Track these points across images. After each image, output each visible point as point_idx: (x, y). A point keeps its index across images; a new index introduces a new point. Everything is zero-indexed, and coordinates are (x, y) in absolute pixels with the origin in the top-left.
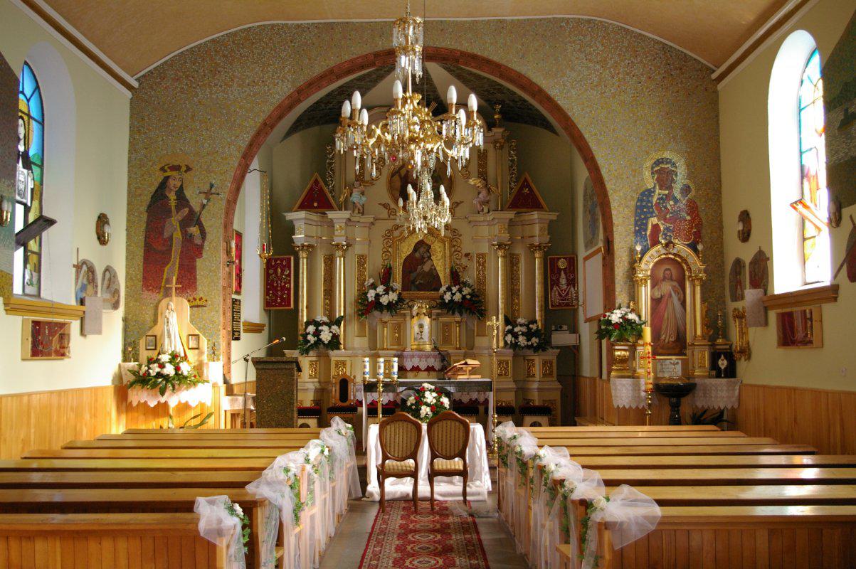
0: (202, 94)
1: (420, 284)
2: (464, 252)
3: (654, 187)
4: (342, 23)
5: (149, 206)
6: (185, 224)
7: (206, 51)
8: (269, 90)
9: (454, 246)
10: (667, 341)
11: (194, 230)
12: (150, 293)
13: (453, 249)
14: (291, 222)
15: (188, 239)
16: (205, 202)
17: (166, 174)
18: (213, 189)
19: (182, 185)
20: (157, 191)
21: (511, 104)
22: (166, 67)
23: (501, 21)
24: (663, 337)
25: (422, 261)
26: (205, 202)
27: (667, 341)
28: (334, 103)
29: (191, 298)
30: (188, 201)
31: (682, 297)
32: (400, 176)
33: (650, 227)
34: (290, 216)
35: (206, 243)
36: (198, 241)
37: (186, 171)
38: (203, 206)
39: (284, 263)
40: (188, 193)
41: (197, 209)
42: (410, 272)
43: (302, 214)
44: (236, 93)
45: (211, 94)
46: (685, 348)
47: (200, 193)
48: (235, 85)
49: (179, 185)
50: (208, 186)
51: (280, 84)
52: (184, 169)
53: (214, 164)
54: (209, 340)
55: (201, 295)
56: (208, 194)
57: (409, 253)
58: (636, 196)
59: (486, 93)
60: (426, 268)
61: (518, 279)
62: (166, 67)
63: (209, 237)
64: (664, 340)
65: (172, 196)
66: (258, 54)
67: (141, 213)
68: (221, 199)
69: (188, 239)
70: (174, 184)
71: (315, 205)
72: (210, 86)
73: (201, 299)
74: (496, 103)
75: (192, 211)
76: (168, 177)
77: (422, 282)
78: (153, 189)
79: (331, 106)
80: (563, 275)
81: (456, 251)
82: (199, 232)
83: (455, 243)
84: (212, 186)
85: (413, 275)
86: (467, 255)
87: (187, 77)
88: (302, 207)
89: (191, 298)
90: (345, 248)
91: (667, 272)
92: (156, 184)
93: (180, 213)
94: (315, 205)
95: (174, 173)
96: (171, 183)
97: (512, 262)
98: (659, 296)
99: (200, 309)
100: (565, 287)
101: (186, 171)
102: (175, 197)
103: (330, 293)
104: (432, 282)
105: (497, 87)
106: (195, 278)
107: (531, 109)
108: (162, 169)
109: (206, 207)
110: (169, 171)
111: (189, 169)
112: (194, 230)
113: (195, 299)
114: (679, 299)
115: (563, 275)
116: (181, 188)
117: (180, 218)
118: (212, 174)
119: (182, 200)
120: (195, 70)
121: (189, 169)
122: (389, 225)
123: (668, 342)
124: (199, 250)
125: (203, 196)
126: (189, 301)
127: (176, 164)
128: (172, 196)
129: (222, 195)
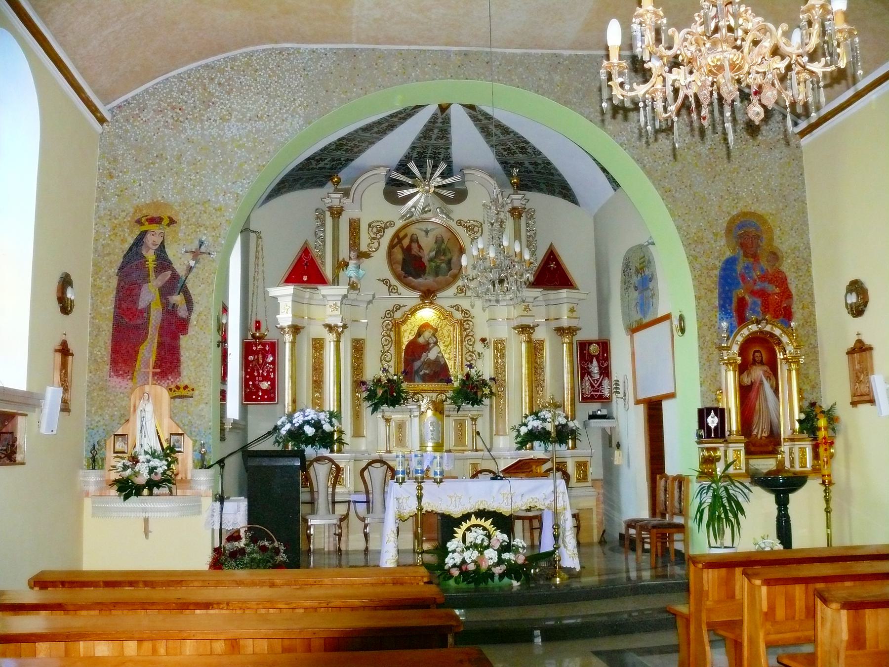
0: (191, 129)
1: (425, 374)
2: (478, 337)
4: (368, 49)
5: (121, 269)
6: (166, 291)
7: (198, 79)
8: (276, 125)
9: (466, 330)
10: (759, 436)
11: (177, 299)
12: (120, 379)
13: (465, 334)
14: (275, 298)
15: (170, 311)
16: (192, 263)
17: (143, 228)
18: (203, 247)
19: (162, 243)
20: (131, 249)
21: (531, 167)
22: (147, 96)
23: (556, 55)
24: (755, 433)
25: (426, 347)
26: (192, 263)
27: (759, 436)
28: (326, 162)
29: (173, 386)
30: (170, 263)
32: (402, 247)
33: (735, 300)
34: (274, 292)
35: (194, 317)
36: (182, 312)
37: (168, 225)
38: (190, 269)
39: (267, 348)
40: (170, 252)
41: (181, 271)
42: (414, 360)
43: (290, 289)
44: (234, 130)
45: (202, 128)
46: (779, 444)
47: (186, 252)
48: (233, 120)
50: (197, 243)
51: (290, 120)
53: (205, 216)
54: (195, 442)
55: (186, 382)
56: (196, 254)
57: (411, 338)
59: (505, 153)
60: (432, 355)
61: (542, 368)
62: (147, 96)
63: (196, 308)
65: (150, 256)
66: (263, 83)
67: (110, 277)
68: (213, 261)
69: (170, 311)
70: (152, 240)
71: (305, 278)
72: (202, 121)
73: (186, 387)
74: (512, 167)
75: (175, 277)
77: (427, 372)
78: (127, 246)
79: (322, 164)
80: (595, 362)
81: (467, 335)
82: (184, 302)
83: (466, 327)
84: (201, 243)
85: (417, 364)
86: (483, 340)
87: (173, 108)
88: (289, 280)
89: (173, 386)
90: (340, 330)
91: (757, 354)
92: (131, 241)
93: (159, 277)
94: (305, 278)
95: (153, 227)
96: (150, 239)
97: (535, 349)
98: (749, 383)
99: (185, 400)
100: (597, 376)
101: (168, 225)
102: (154, 257)
103: (318, 384)
104: (439, 372)
105: (522, 145)
106: (178, 361)
107: (552, 174)
108: (139, 222)
109: (194, 270)
110: (147, 223)
111: (172, 222)
112: (177, 299)
113: (178, 388)
114: (772, 387)
115: (595, 362)
116: (162, 245)
117: (160, 284)
118: (202, 229)
119: (163, 263)
120: (183, 100)
121: (172, 222)
122: (389, 305)
124: (182, 326)
125: (189, 256)
126: (170, 390)
127: (155, 215)
128: (150, 256)
129: (214, 255)
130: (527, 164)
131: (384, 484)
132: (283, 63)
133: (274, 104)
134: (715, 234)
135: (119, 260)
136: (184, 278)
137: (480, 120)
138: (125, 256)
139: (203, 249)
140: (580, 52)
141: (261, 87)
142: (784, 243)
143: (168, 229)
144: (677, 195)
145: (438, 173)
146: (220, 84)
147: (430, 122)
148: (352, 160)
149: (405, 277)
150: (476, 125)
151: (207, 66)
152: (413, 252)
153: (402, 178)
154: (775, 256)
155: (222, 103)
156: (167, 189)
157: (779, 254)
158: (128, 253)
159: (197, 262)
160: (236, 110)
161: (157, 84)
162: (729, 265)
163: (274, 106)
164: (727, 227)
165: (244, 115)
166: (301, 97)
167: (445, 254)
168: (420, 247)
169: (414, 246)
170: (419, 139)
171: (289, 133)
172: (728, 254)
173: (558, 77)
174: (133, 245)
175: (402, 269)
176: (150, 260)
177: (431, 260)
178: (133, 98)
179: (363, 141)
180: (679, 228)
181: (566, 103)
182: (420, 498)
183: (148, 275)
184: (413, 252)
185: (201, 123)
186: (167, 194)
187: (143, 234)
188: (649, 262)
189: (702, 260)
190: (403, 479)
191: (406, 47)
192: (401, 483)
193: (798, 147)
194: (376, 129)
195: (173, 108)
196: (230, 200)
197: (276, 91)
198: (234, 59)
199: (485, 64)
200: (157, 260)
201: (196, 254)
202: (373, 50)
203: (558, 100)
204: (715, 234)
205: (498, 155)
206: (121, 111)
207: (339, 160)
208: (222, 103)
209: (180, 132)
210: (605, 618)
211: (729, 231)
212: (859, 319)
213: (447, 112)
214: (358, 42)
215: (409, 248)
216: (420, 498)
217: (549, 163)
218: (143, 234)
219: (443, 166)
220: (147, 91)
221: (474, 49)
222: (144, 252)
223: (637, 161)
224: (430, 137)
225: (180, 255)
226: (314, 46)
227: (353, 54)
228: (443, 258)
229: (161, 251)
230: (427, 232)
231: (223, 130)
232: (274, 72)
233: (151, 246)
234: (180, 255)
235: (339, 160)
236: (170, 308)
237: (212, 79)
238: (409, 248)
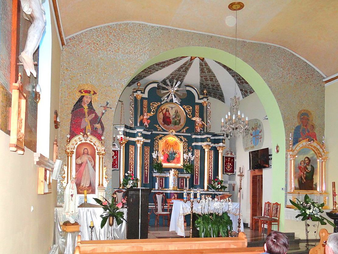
3: (301, 125)
5: (73, 111)
6: (93, 122)
17: (82, 95)
18: (108, 105)
20: (77, 103)
26: (104, 111)
30: (94, 110)
31: (93, 164)
32: (163, 113)
37: (93, 94)
40: (94, 106)
41: (99, 115)
48: (120, 52)
49: (90, 101)
51: (143, 55)
52: (92, 93)
56: (105, 108)
58: (294, 128)
64: (83, 186)
65: (86, 107)
68: (113, 111)
70: (86, 100)
72: (107, 51)
75: (96, 116)
76: (84, 96)
78: (75, 102)
87: (94, 43)
93: (90, 116)
95: (87, 94)
96: (85, 99)
101: (93, 94)
102: (87, 108)
108: (80, 91)
110: (84, 92)
111: (95, 93)
112: (98, 126)
114: (92, 165)
117: (90, 119)
119: (91, 109)
121: (95, 93)
123: (85, 187)
125: (103, 108)
128: (86, 107)
130: (210, 85)
131: (69, 202)
132: (140, 30)
133: (137, 48)
134: (294, 117)
135: (71, 107)
136: (100, 117)
137: (202, 66)
138: (74, 106)
139: (108, 106)
140: (253, 42)
141: (132, 40)
142: (316, 122)
143: (93, 96)
144: (282, 101)
145: (177, 86)
146: (114, 36)
147: (184, 64)
148: (146, 77)
149: (164, 124)
150: (209, 67)
151: (109, 26)
152: (167, 115)
153: (164, 86)
154: (313, 127)
155: (115, 44)
156: (92, 78)
157: (314, 126)
158: (76, 104)
159: (106, 111)
160: (121, 48)
161: (87, 31)
162: (298, 128)
163: (137, 49)
164: (298, 115)
165: (125, 51)
166: (148, 46)
167: (178, 117)
168: (169, 114)
169: (167, 113)
170: (176, 71)
171: (143, 61)
172: (298, 125)
173: (244, 51)
174: (78, 101)
175: (163, 121)
176: (86, 109)
177: (173, 119)
178: (76, 36)
179: (154, 69)
180: (282, 114)
181: (246, 62)
182: (192, 208)
183: (85, 115)
184: (167, 115)
185: (106, 52)
186: (93, 81)
187: (83, 97)
188: (260, 125)
189: (288, 126)
190: (186, 201)
191: (189, 31)
192: (185, 202)
193: (324, 87)
194: (162, 65)
195: (94, 43)
196: (119, 86)
197: (138, 42)
198: (120, 25)
199: (218, 42)
200: (88, 109)
201: (105, 108)
202: (176, 30)
203: (243, 60)
204: (294, 117)
205: (201, 80)
206: (71, 41)
207: (141, 76)
208: (115, 44)
209: (98, 55)
210: (73, 241)
211: (298, 116)
212: (279, 152)
213: (193, 61)
214: (171, 26)
215: (165, 114)
216: (192, 208)
217: (219, 86)
218: (83, 97)
219: (179, 83)
220: (82, 33)
221: (215, 35)
222: (83, 105)
223: (270, 87)
224: (180, 71)
225: (98, 108)
226: (154, 25)
227: (169, 30)
228: (178, 118)
229: (90, 104)
230: (172, 108)
231: (116, 56)
232: (137, 34)
233: (86, 103)
234: (98, 108)
235: (141, 76)
236: (94, 129)
237: (111, 33)
238: (165, 114)
